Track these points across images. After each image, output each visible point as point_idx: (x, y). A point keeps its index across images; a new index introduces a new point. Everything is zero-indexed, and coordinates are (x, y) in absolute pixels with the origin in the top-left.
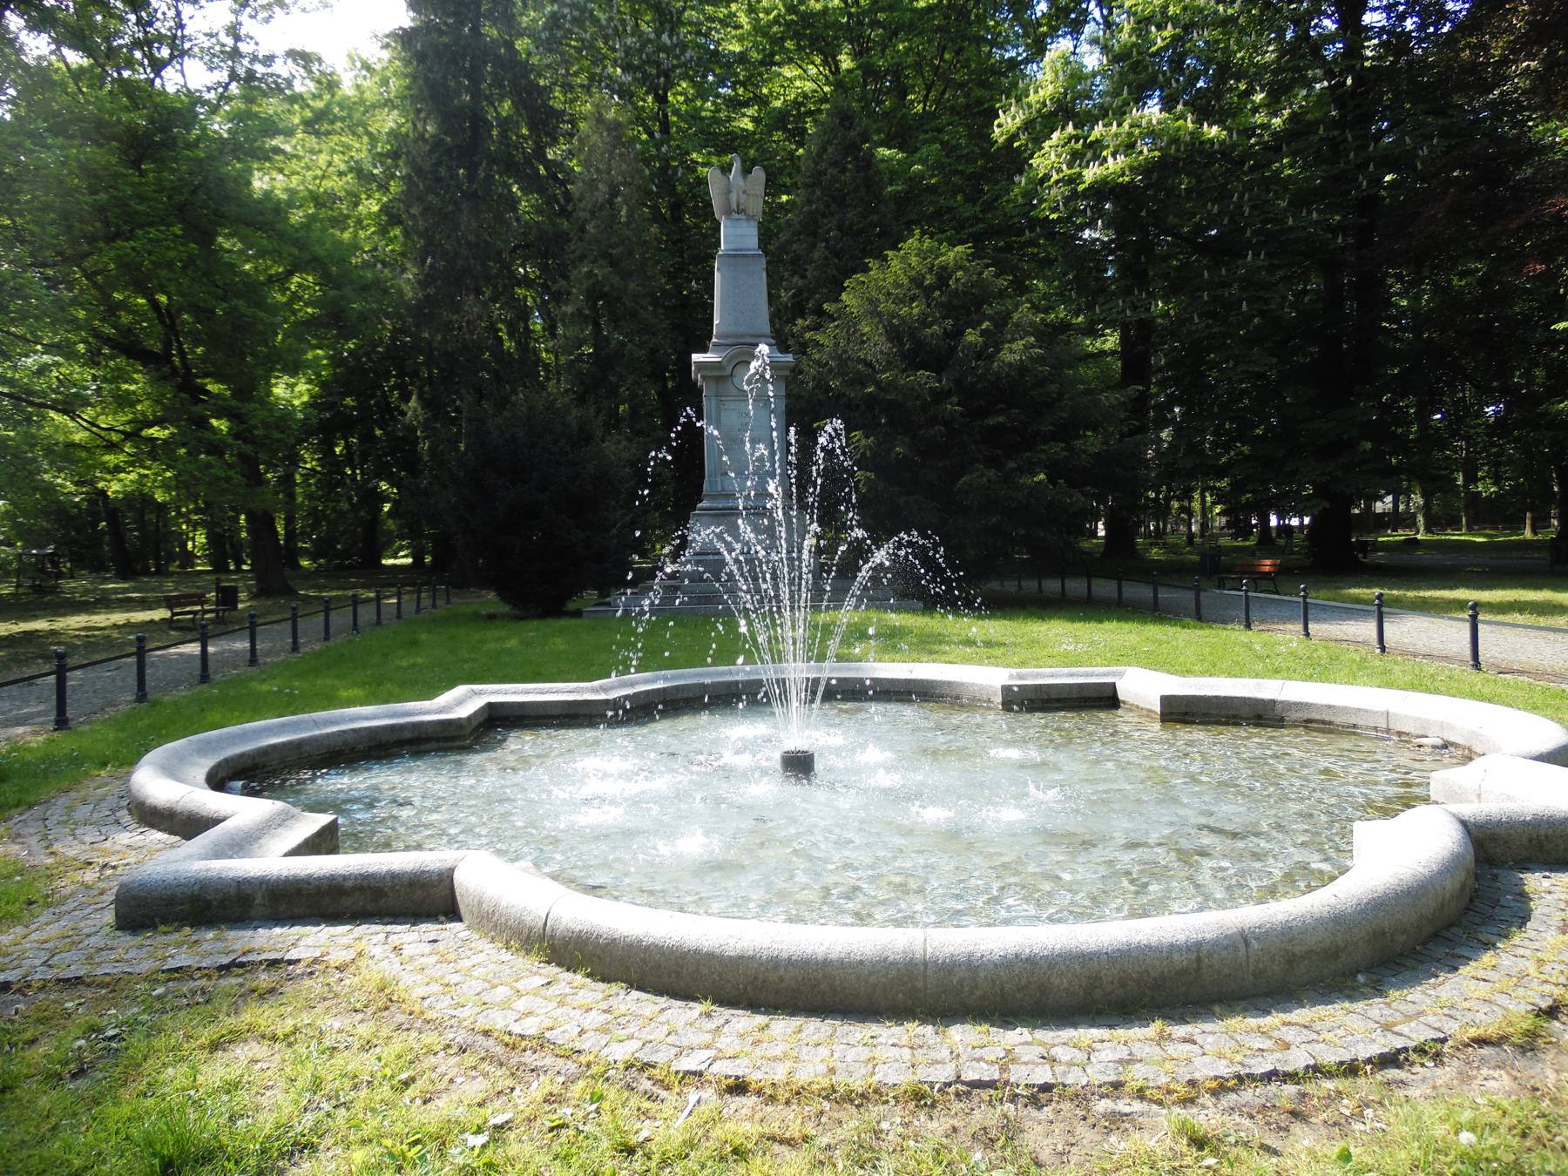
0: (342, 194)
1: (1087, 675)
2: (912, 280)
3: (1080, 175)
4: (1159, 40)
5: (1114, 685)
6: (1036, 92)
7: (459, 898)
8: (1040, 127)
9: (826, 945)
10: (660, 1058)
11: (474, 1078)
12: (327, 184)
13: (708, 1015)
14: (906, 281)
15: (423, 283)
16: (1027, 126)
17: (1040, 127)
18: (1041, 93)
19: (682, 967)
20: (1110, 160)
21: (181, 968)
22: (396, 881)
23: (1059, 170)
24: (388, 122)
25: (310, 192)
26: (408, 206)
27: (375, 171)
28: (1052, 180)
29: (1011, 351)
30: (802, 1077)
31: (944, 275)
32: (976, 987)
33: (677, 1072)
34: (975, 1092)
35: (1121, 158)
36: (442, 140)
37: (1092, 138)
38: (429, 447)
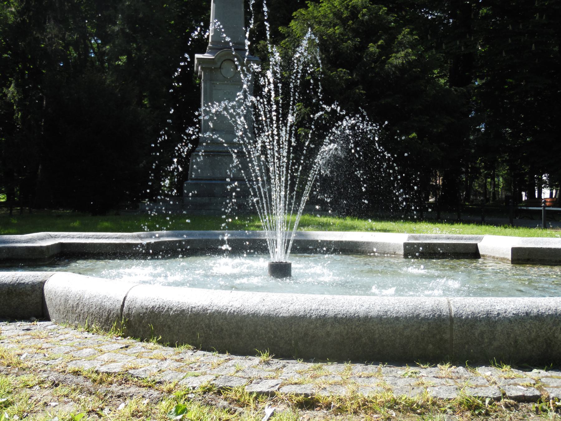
2: (335, 14)
5: (476, 245)
7: (48, 302)
9: (366, 306)
10: (235, 384)
13: (267, 363)
14: (331, 15)
19: (242, 329)
29: (396, 58)
33: (251, 393)
34: (521, 405)
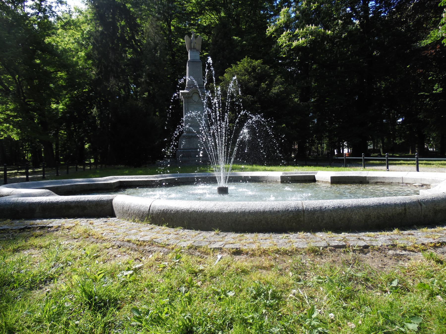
0: (73, 50)
1: (306, 173)
2: (245, 70)
3: (292, 44)
4: (313, 7)
5: (314, 176)
6: (279, 21)
7: (114, 209)
8: (279, 31)
9: (264, 206)
10: (203, 244)
11: (125, 255)
12: (68, 46)
13: (218, 234)
14: (243, 70)
15: (97, 74)
16: (276, 31)
17: (279, 31)
18: (280, 21)
20: (300, 40)
21: (4, 229)
22: (91, 204)
23: (286, 43)
24: (87, 28)
25: (64, 48)
26: (94, 51)
27: (83, 43)
28: (284, 46)
29: (275, 89)
30: (265, 247)
31: (254, 68)
32: (324, 219)
35: (303, 39)
36: (103, 32)
37: (295, 33)
38: (100, 122)
